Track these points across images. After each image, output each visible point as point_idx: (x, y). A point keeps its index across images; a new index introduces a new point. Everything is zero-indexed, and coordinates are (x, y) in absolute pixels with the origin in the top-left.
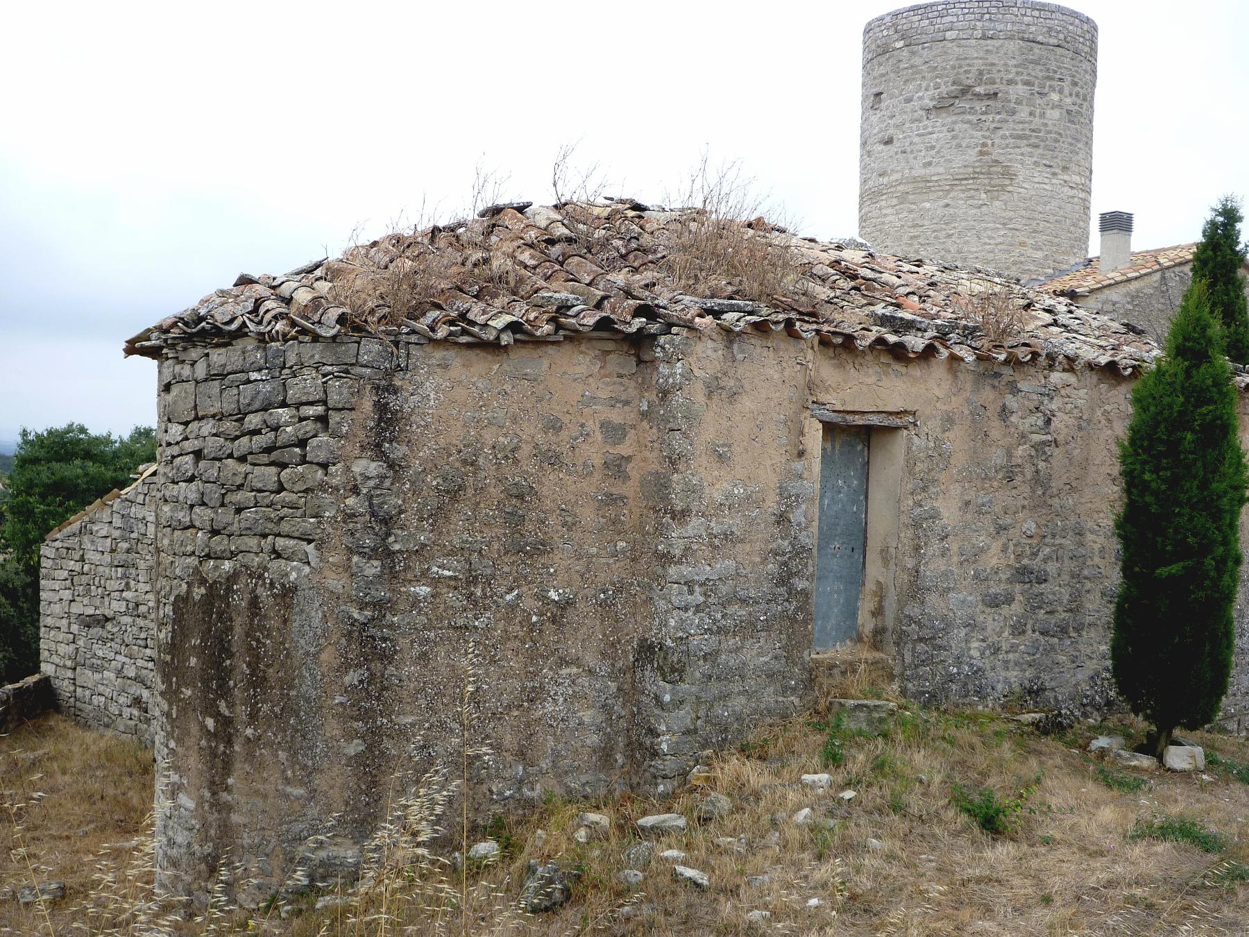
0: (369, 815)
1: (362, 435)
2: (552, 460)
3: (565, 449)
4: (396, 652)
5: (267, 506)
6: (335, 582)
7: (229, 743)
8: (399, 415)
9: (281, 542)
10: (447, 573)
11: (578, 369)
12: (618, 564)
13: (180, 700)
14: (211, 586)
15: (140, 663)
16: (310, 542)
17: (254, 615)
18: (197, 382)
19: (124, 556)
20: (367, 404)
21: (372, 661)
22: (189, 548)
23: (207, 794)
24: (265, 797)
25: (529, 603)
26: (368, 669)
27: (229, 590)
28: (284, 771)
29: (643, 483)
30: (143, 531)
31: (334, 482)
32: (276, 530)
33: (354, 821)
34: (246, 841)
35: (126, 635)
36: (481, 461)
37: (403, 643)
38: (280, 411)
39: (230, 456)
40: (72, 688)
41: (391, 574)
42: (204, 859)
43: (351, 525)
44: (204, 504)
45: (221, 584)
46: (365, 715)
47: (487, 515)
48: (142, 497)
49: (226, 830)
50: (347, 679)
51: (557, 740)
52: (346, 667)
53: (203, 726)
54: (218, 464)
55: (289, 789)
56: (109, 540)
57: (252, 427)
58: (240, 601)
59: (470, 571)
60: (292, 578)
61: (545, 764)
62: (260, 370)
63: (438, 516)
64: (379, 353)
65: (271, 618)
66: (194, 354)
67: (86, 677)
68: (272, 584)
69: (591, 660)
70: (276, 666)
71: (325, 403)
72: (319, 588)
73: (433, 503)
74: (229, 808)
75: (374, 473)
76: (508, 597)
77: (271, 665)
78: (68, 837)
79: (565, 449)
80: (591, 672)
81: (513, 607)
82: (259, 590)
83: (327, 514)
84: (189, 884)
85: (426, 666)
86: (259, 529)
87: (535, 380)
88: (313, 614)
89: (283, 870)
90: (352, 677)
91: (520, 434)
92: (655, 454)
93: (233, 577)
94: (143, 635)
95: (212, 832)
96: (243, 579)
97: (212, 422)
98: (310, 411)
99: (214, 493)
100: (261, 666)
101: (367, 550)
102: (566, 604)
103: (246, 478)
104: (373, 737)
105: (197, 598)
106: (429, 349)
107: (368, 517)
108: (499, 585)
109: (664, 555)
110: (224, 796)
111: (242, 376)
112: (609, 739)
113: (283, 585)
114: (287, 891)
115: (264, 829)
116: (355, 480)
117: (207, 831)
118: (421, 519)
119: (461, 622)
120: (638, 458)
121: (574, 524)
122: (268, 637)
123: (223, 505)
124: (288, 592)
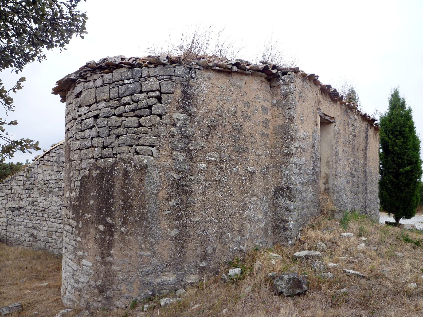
0: (181, 261)
1: (177, 103)
2: (247, 118)
3: (251, 114)
4: (192, 191)
5: (133, 133)
6: (165, 163)
7: (112, 235)
8: (192, 96)
9: (139, 148)
10: (212, 159)
11: (254, 86)
12: (267, 159)
13: (84, 220)
14: (103, 169)
15: (34, 222)
16: (153, 147)
17: (126, 179)
18: (96, 88)
19: (29, 186)
20: (179, 91)
21: (182, 195)
22: (90, 156)
23: (99, 259)
24: (131, 257)
25: (241, 172)
26: (180, 199)
27: (112, 170)
28: (140, 245)
29: (275, 129)
30: (36, 177)
31: (165, 122)
32: (137, 143)
33: (174, 264)
34: (120, 277)
35: (28, 213)
36: (224, 115)
37: (195, 187)
38: (139, 94)
39: (114, 115)
40: (5, 233)
41: (190, 159)
42: (97, 287)
43: (173, 139)
44: (99, 136)
45: (108, 168)
46: (179, 218)
47: (227, 136)
48: (37, 165)
49: (109, 273)
50: (171, 204)
51: (251, 226)
52: (171, 198)
53: (97, 230)
54: (107, 119)
55: (142, 253)
56: (23, 181)
57: (125, 102)
58: (118, 173)
59: (221, 158)
60: (145, 162)
61: (247, 235)
62: (129, 79)
63: (208, 136)
64: (184, 72)
65: (134, 180)
66: (95, 77)
67: (12, 228)
68: (135, 165)
69: (261, 195)
70: (137, 200)
71: (160, 91)
72: (158, 166)
73: (207, 130)
74: (111, 264)
75: (182, 118)
76: (234, 169)
77: (135, 200)
78: (17, 284)
79: (251, 114)
80: (261, 199)
81: (236, 173)
82: (128, 169)
83: (162, 135)
84: (88, 299)
85: (204, 197)
86: (129, 143)
87: (241, 87)
88: (155, 176)
89: (139, 289)
90: (173, 203)
91: (237, 106)
92: (281, 118)
93: (116, 164)
94: (35, 212)
95: (102, 275)
96: (120, 165)
97: (104, 102)
98: (153, 94)
99: (105, 131)
100: (129, 201)
101: (179, 149)
102: (253, 173)
103: (122, 123)
104: (183, 227)
105: (94, 175)
106: (203, 71)
107: (180, 136)
108: (231, 164)
109: (288, 154)
110: (109, 259)
111: (122, 82)
112: (267, 225)
113: (141, 166)
114: (141, 298)
115: (129, 271)
116: (174, 121)
117: (98, 275)
118: (202, 137)
119: (218, 179)
120: (272, 120)
121: (255, 142)
122: (132, 188)
123: (109, 135)
124: (143, 169)
